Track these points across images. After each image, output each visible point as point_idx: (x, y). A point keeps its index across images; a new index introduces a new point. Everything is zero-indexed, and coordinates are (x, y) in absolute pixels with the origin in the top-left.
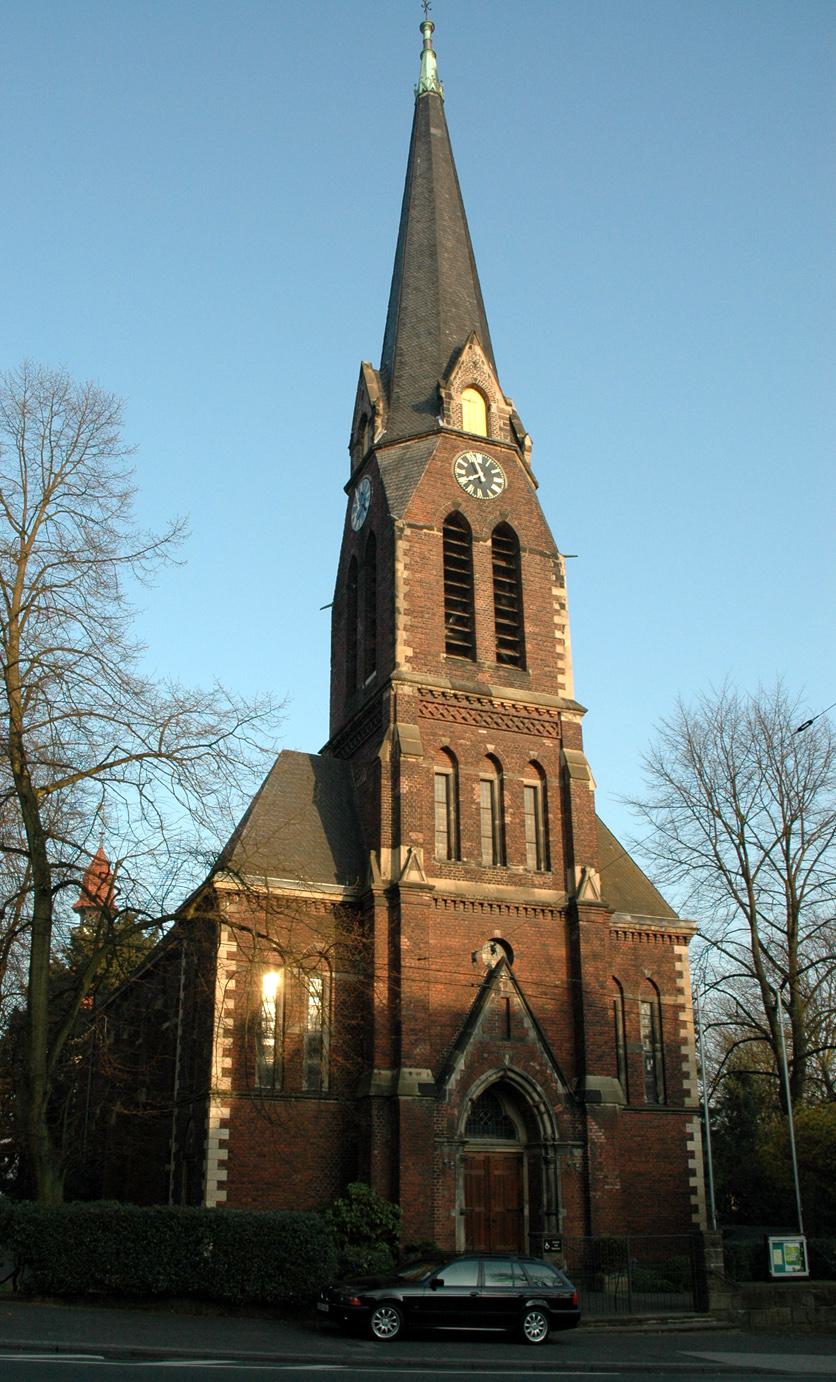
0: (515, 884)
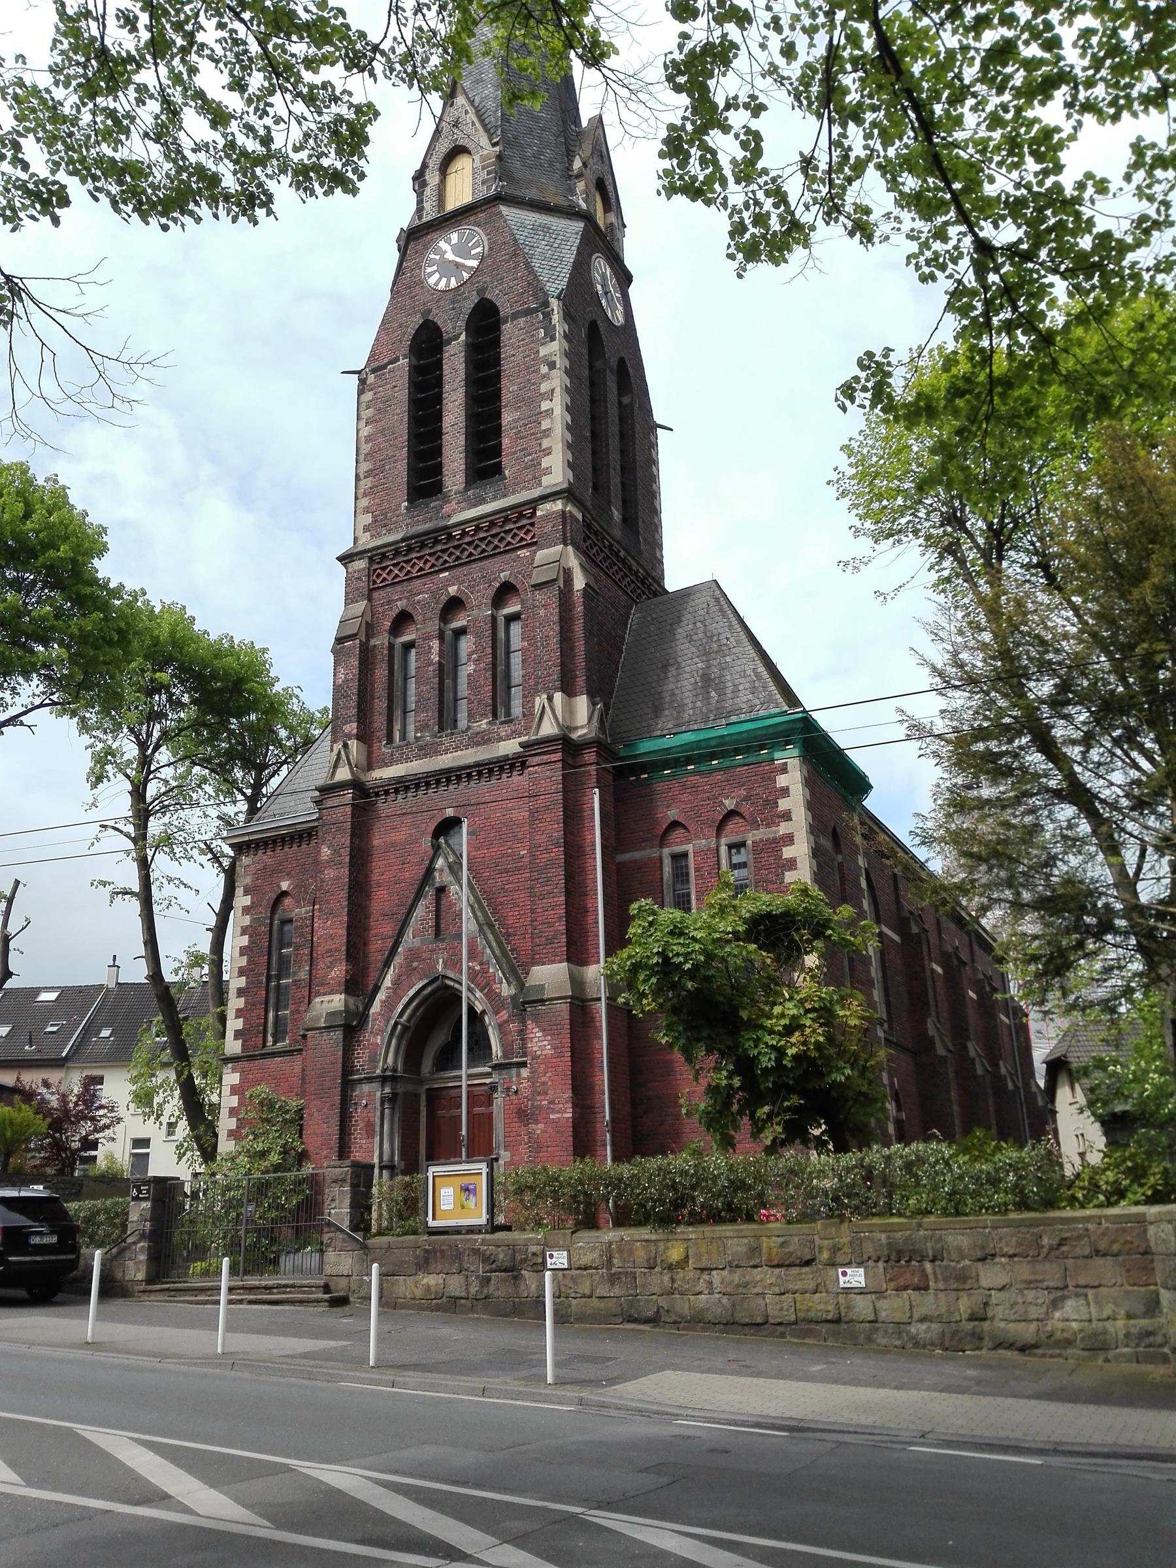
0: (477, 744)
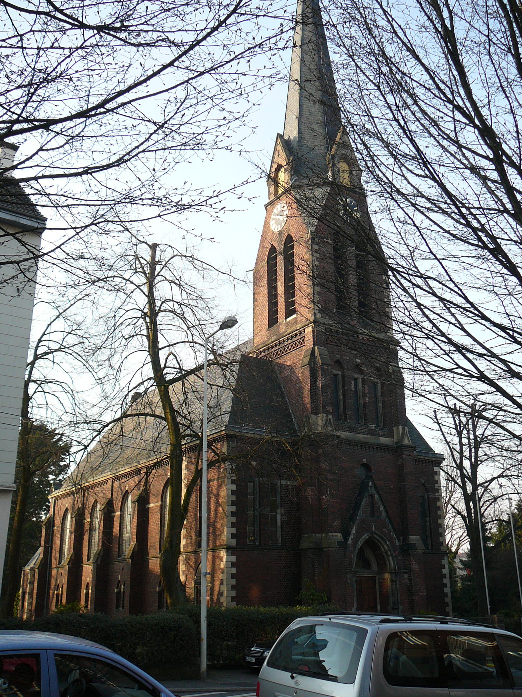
0: (371, 434)
